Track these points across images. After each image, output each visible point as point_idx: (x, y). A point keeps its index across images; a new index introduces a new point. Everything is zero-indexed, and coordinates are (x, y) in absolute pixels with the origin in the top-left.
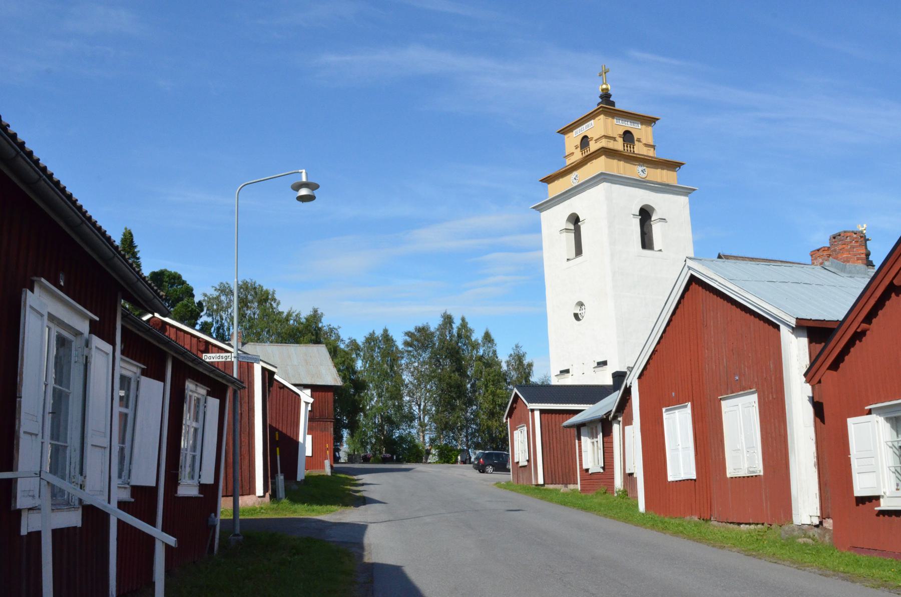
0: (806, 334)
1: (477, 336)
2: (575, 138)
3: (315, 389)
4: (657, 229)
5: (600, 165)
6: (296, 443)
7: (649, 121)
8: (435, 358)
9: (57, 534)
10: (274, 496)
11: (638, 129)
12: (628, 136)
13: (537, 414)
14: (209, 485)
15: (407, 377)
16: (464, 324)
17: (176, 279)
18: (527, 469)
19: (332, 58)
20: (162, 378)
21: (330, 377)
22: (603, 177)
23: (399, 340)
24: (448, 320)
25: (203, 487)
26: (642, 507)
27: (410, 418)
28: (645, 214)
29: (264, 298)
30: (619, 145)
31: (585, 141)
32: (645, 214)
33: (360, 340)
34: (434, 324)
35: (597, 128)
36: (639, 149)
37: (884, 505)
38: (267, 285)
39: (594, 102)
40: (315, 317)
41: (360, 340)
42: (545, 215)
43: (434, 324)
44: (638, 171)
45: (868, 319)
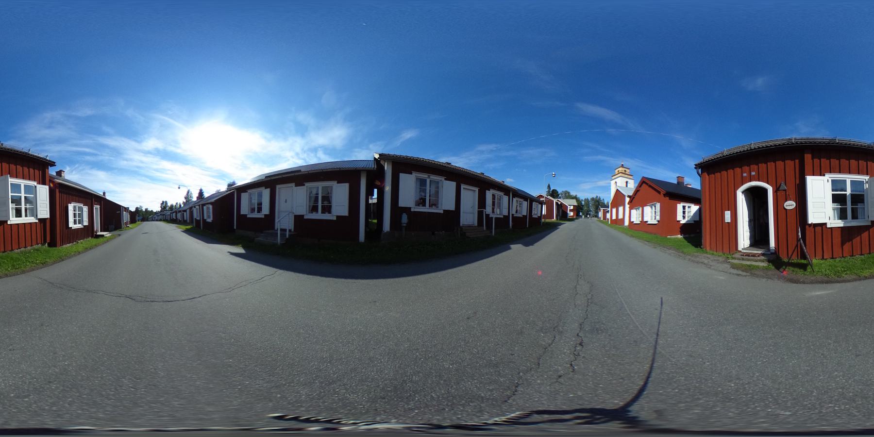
0: (391, 163)
1: (602, 199)
2: (617, 170)
3: (574, 206)
4: (628, 184)
5: (620, 175)
6: (567, 213)
7: (629, 169)
8: (595, 203)
9: (25, 194)
10: (557, 219)
11: (627, 170)
12: (625, 171)
13: (602, 210)
14: (452, 211)
15: (590, 205)
16: (600, 198)
17: (556, 190)
18: (600, 218)
19: (586, 157)
20: (527, 201)
21: (576, 204)
22: (620, 176)
23: (589, 199)
24: (597, 197)
25: (539, 217)
26: (609, 223)
27: (591, 211)
28: (627, 182)
29: (569, 193)
30: (624, 172)
31: (619, 171)
32: (627, 182)
33: (583, 199)
34: (595, 197)
35: (621, 169)
36: (627, 173)
37: (649, 223)
38: (569, 191)
39: (621, 166)
40: (576, 196)
41: (583, 199)
42: (612, 181)
43: (595, 197)
44: (626, 176)
45: (635, 195)
